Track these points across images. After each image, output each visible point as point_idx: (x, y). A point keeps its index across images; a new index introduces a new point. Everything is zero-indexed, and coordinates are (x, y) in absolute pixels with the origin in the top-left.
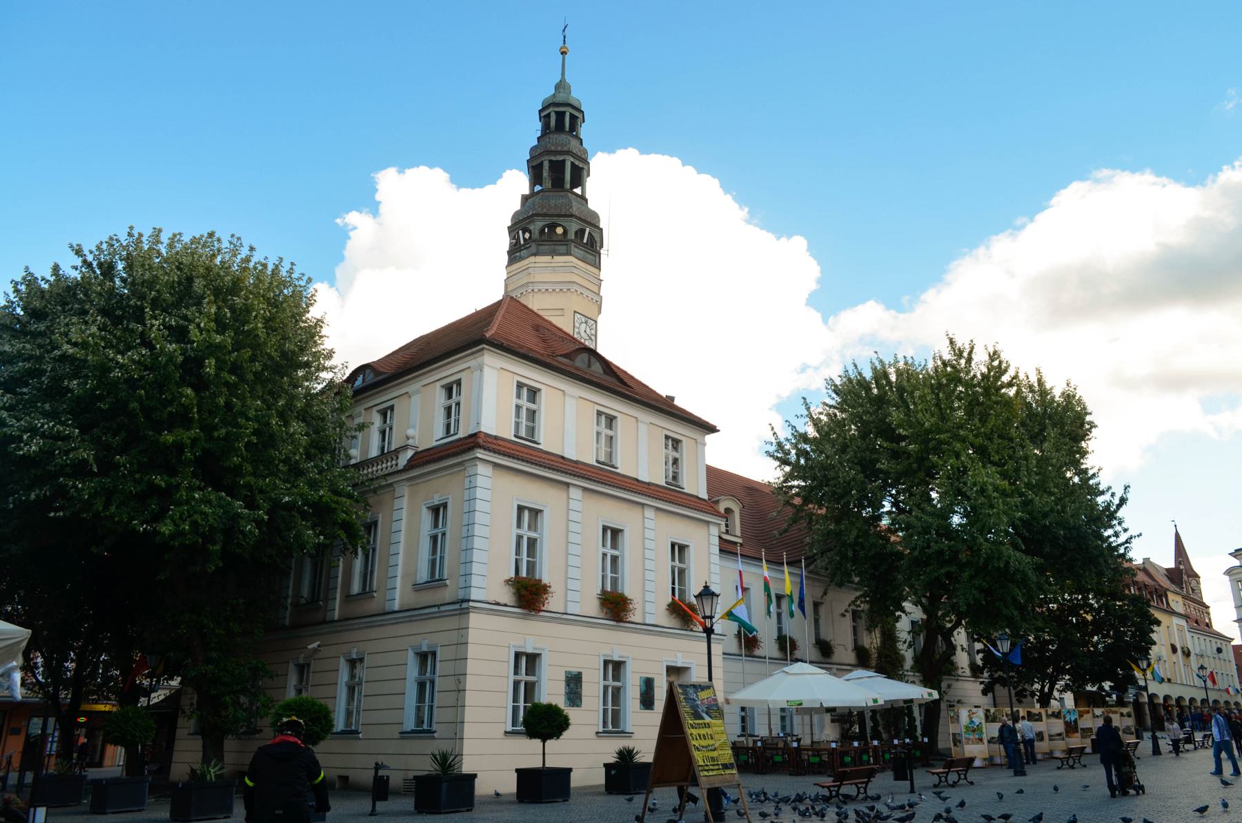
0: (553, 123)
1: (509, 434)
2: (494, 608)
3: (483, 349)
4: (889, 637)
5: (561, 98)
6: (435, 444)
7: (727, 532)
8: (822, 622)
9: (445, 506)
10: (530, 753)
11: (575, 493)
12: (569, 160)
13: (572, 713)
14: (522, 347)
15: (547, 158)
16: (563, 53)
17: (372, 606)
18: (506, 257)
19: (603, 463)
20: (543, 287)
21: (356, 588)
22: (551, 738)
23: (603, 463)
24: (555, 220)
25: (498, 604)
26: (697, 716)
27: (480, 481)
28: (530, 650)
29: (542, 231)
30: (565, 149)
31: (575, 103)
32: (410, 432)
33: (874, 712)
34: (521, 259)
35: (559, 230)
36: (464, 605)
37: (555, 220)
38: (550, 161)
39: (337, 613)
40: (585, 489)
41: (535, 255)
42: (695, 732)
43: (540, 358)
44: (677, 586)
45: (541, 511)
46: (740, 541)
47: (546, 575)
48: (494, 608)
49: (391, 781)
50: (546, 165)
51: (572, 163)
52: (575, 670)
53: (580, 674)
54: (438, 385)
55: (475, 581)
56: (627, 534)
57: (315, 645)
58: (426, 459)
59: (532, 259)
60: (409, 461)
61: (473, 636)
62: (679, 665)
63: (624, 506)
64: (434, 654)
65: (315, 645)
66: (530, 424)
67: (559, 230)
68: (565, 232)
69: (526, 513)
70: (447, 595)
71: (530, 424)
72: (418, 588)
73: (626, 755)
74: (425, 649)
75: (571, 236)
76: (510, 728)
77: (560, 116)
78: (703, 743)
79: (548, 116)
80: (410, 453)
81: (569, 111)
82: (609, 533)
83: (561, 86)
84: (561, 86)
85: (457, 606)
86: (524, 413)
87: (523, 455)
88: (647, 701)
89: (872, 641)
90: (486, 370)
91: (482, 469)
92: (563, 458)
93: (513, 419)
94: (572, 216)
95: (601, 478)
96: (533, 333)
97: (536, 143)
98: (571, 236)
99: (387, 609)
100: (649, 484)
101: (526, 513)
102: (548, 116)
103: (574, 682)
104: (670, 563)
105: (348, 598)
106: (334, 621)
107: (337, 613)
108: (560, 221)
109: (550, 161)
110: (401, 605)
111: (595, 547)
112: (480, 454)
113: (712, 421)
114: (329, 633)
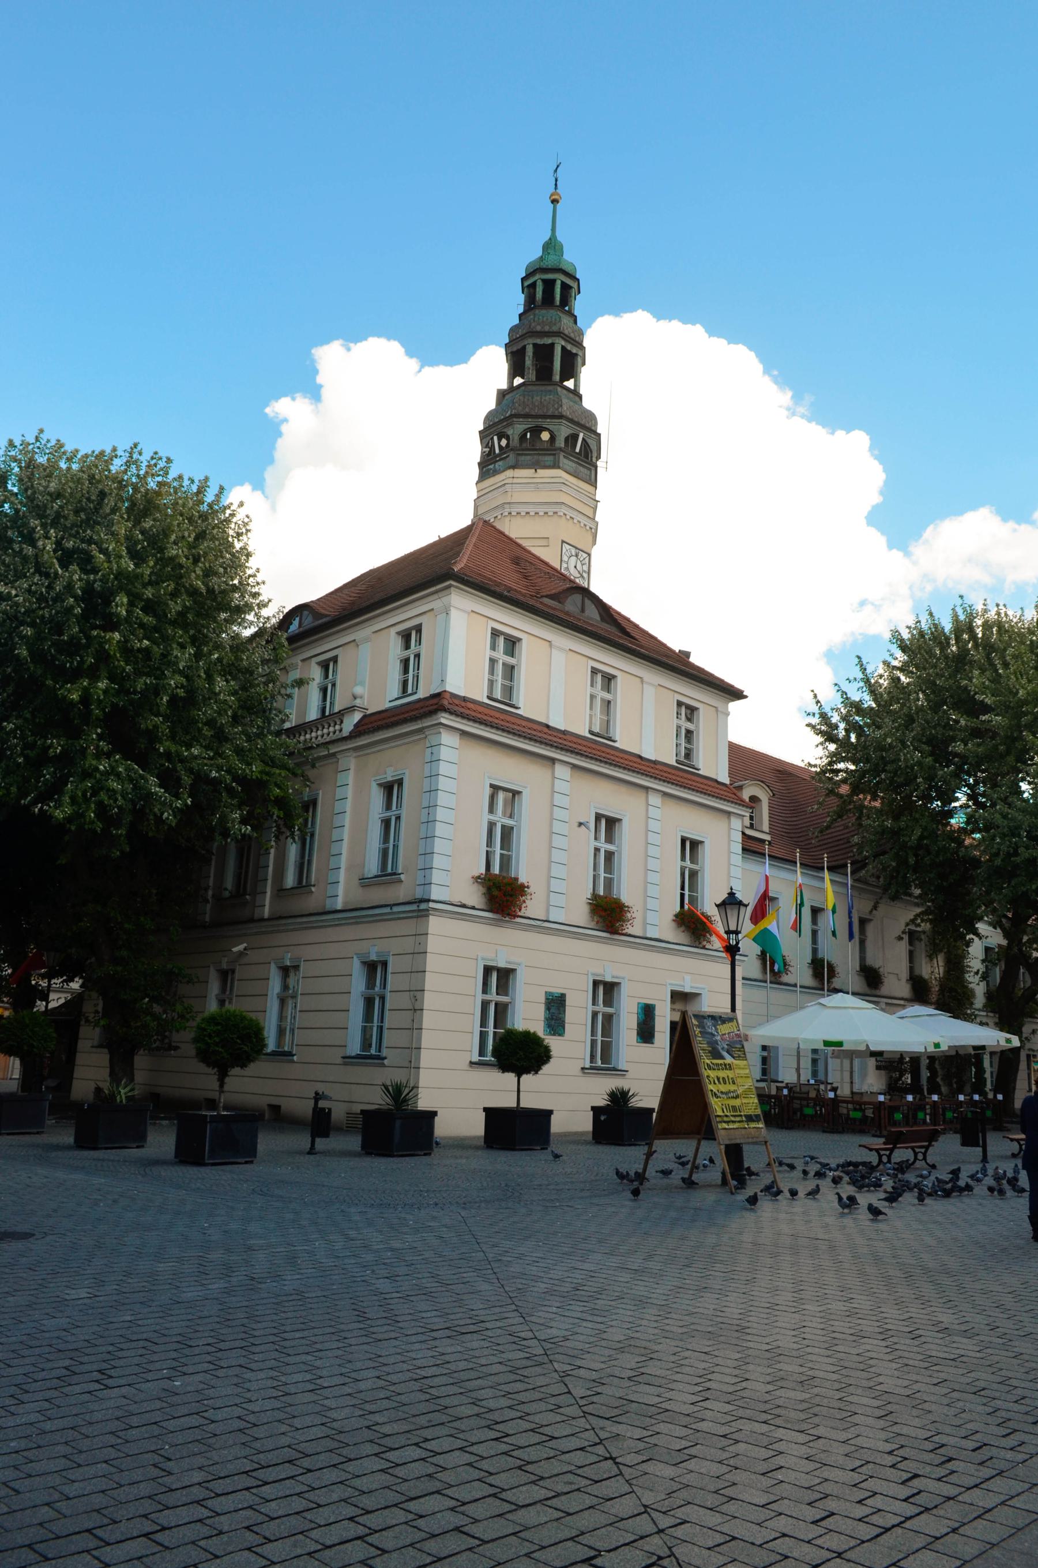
2: (459, 910)
3: (449, 587)
4: (956, 966)
5: (551, 261)
6: (388, 705)
8: (869, 944)
9: (400, 782)
10: (502, 1089)
12: (559, 344)
13: (553, 1043)
15: (531, 341)
16: (554, 202)
17: (312, 903)
22: (528, 1072)
24: (540, 422)
25: (464, 906)
26: (716, 1054)
27: (445, 753)
28: (502, 964)
29: (523, 437)
30: (555, 329)
32: (358, 690)
33: (932, 1058)
34: (496, 472)
35: (545, 436)
36: (423, 906)
37: (540, 422)
38: (535, 345)
42: (712, 1074)
44: (687, 892)
46: (768, 838)
48: (459, 910)
49: (554, 1118)
51: (563, 348)
52: (557, 991)
53: (563, 996)
54: (393, 631)
55: (436, 877)
56: (626, 824)
58: (376, 724)
59: (510, 473)
60: (357, 726)
61: (433, 944)
62: (687, 990)
63: (623, 789)
66: (507, 683)
67: (545, 436)
68: (553, 438)
69: (501, 796)
70: (401, 893)
71: (507, 683)
72: (366, 882)
73: (619, 1098)
75: (560, 443)
77: (549, 285)
78: (723, 1088)
79: (533, 285)
80: (357, 717)
81: (560, 278)
82: (603, 822)
83: (552, 245)
84: (552, 245)
85: (414, 907)
86: (499, 668)
88: (646, 1033)
89: (933, 970)
90: (453, 613)
93: (487, 676)
94: (561, 417)
95: (595, 752)
98: (560, 443)
99: (329, 905)
102: (533, 285)
103: (556, 1005)
105: (280, 892)
106: (262, 920)
108: (546, 423)
109: (535, 345)
110: (345, 903)
112: (445, 719)
114: (256, 934)
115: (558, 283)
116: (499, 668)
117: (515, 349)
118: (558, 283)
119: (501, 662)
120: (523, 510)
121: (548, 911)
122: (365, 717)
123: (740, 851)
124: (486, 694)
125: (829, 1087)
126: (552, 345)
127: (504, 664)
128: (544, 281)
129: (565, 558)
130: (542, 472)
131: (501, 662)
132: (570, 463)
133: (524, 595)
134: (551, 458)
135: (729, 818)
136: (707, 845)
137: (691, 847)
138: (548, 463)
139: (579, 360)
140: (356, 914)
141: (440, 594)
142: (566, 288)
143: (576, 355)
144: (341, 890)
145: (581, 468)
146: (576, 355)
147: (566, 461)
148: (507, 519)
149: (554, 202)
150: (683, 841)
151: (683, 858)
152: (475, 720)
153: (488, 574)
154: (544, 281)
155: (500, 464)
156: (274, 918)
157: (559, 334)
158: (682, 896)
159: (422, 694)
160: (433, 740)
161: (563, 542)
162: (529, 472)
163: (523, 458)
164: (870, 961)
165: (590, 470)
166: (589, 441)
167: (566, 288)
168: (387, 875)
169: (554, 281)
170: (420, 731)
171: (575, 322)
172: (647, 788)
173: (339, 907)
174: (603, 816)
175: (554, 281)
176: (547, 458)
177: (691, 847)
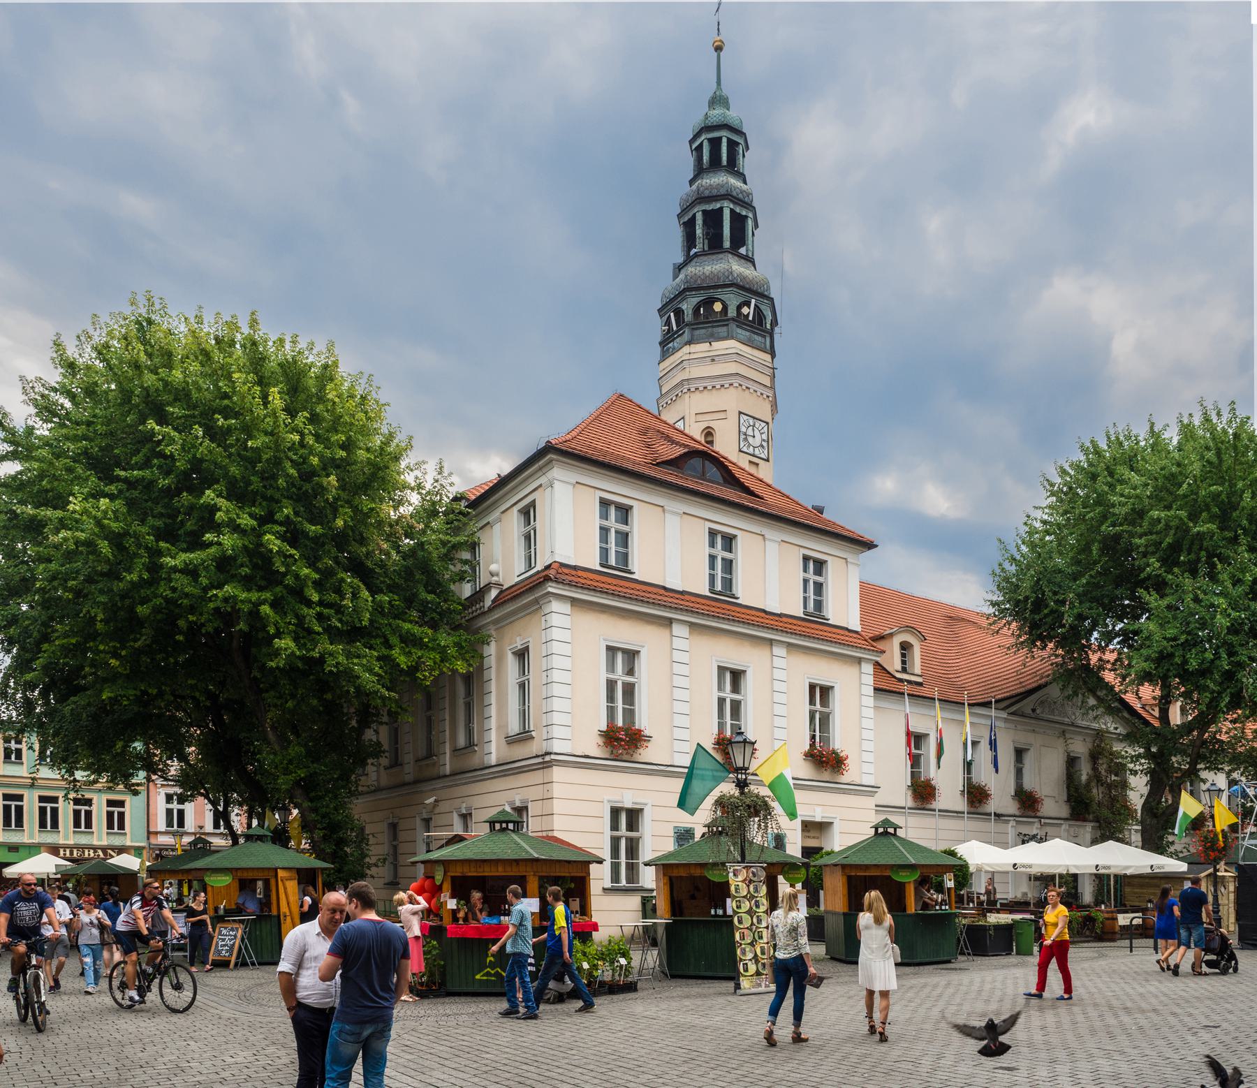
0: (706, 157)
1: (592, 561)
2: (582, 762)
3: (551, 461)
5: (717, 114)
7: (904, 670)
8: (1026, 772)
9: (527, 649)
11: (678, 630)
12: (727, 207)
14: (605, 454)
16: (718, 49)
17: (475, 761)
18: (659, 349)
19: (719, 593)
20: (701, 385)
21: (462, 741)
23: (719, 593)
24: (711, 293)
27: (555, 620)
28: (628, 805)
29: (696, 311)
31: (735, 124)
32: (493, 567)
34: (676, 350)
35: (718, 307)
36: (547, 758)
37: (711, 293)
38: (704, 212)
39: (448, 767)
40: (691, 625)
41: (689, 343)
43: (630, 467)
44: (818, 734)
45: (638, 652)
47: (643, 722)
48: (582, 762)
50: (706, 144)
51: (732, 211)
54: (515, 509)
55: (557, 732)
56: (749, 675)
57: (432, 800)
58: (510, 596)
59: (686, 349)
60: (494, 601)
61: (557, 790)
62: (818, 819)
64: (526, 808)
65: (432, 800)
66: (621, 550)
68: (725, 308)
69: (620, 656)
70: (534, 748)
71: (621, 550)
72: (512, 741)
74: (518, 804)
75: (732, 313)
76: (608, 884)
77: (715, 143)
79: (700, 147)
80: (494, 593)
81: (724, 134)
82: (728, 676)
83: (718, 100)
84: (718, 100)
85: (540, 760)
86: (612, 536)
87: (610, 586)
90: (557, 485)
91: (555, 606)
92: (665, 588)
95: (717, 610)
96: (635, 436)
97: (687, 189)
98: (732, 313)
99: (486, 763)
100: (780, 615)
101: (620, 656)
102: (700, 147)
104: (807, 707)
105: (455, 750)
106: (445, 776)
107: (448, 767)
108: (718, 293)
109: (704, 212)
110: (498, 759)
111: (708, 691)
112: (551, 588)
113: (868, 536)
114: (443, 788)
115: (724, 140)
116: (612, 536)
117: (686, 219)
118: (724, 140)
119: (613, 531)
120: (701, 385)
121: (672, 757)
122: (501, 592)
123: (871, 691)
124: (598, 561)
125: (133, 914)
126: (721, 209)
127: (617, 532)
128: (710, 140)
129: (743, 429)
130: (718, 345)
131: (613, 531)
132: (744, 332)
133: (634, 463)
134: (725, 329)
135: (860, 663)
136: (836, 690)
137: (820, 693)
138: (722, 335)
139: (750, 222)
140: (508, 769)
141: (544, 470)
142: (732, 145)
143: (746, 217)
144: (493, 748)
145: (756, 337)
146: (746, 217)
147: (739, 331)
148: (687, 396)
149: (718, 49)
150: (812, 687)
151: (812, 702)
152: (583, 588)
153: (600, 445)
154: (710, 140)
155: (676, 344)
156: (453, 774)
157: (728, 196)
158: (813, 737)
159: (539, 567)
160: (546, 609)
161: (740, 413)
162: (705, 346)
163: (697, 332)
164: (1028, 785)
165: (764, 337)
166: (762, 307)
167: (732, 145)
168: (524, 736)
169: (720, 139)
170: (536, 601)
171: (745, 182)
172: (771, 640)
173: (493, 762)
174: (727, 668)
175: (720, 139)
176: (720, 329)
177: (820, 693)
